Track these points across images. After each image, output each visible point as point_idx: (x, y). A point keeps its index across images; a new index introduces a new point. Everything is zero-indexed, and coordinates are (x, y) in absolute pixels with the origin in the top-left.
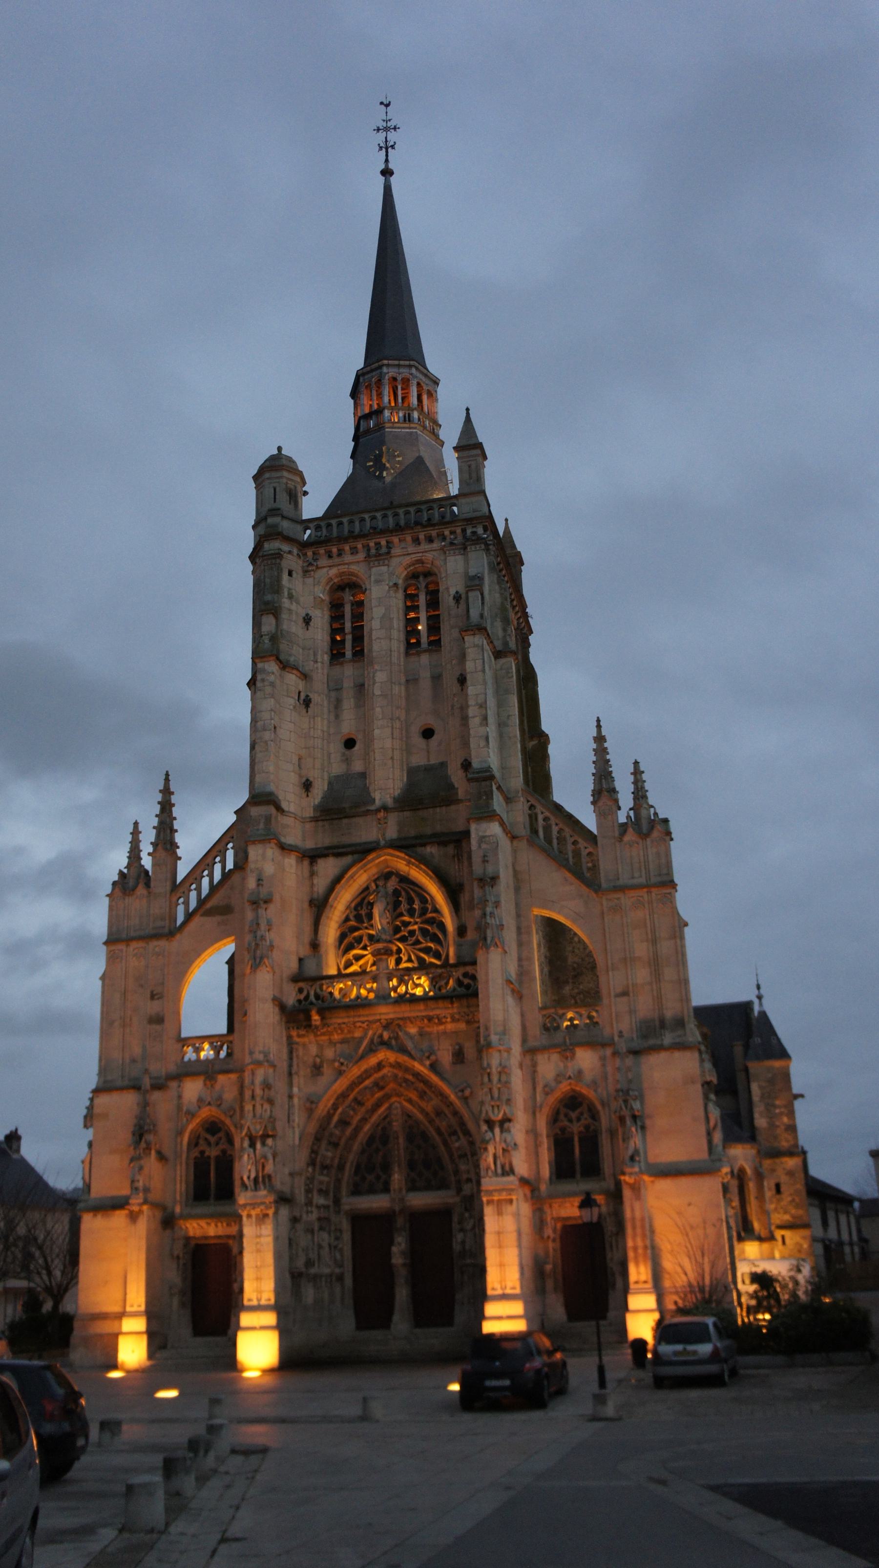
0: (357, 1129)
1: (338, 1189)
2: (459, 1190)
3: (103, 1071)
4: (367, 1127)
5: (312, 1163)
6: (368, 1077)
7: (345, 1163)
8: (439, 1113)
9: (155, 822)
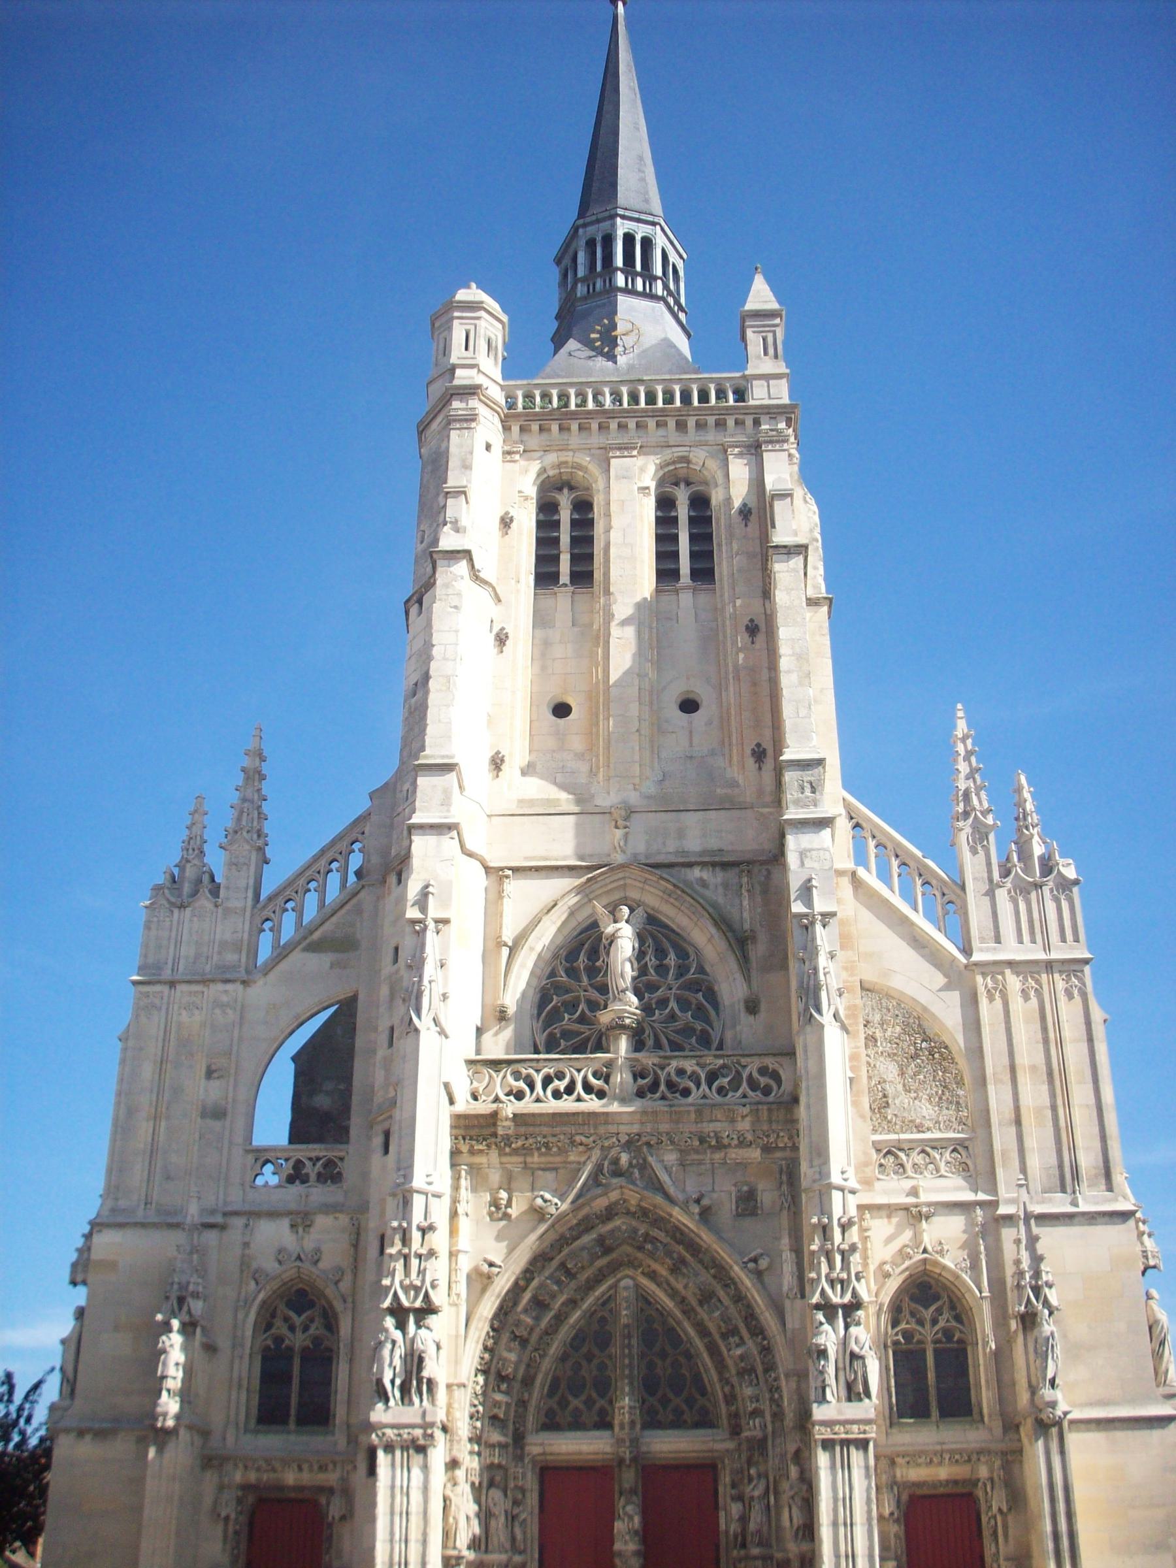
0: (560, 1318)
1: (520, 1418)
2: (735, 1431)
3: (113, 1190)
6: (588, 1230)
7: (536, 1374)
8: (706, 1297)
9: (234, 797)
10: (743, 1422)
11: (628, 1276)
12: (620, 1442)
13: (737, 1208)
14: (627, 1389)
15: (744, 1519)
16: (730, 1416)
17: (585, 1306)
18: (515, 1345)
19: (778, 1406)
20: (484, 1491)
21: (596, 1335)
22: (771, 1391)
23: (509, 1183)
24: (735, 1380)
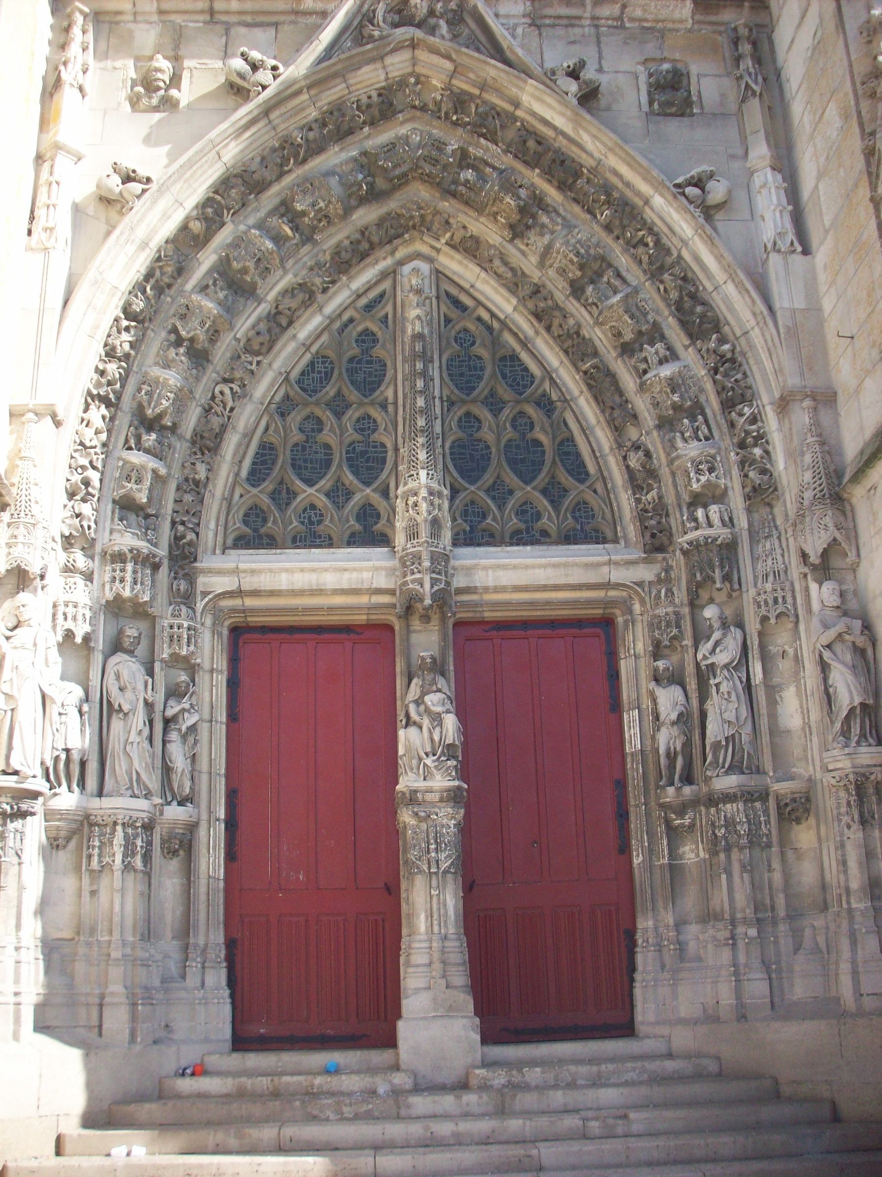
1: (188, 515)
2: (657, 543)
4: (309, 325)
7: (224, 428)
8: (591, 273)
10: (674, 522)
11: (418, 256)
12: (409, 562)
13: (651, 103)
14: (422, 455)
15: (692, 721)
16: (642, 515)
17: (330, 308)
18: (180, 355)
19: (764, 471)
20: (98, 658)
21: (354, 365)
22: (742, 445)
23: (177, 47)
24: (654, 441)
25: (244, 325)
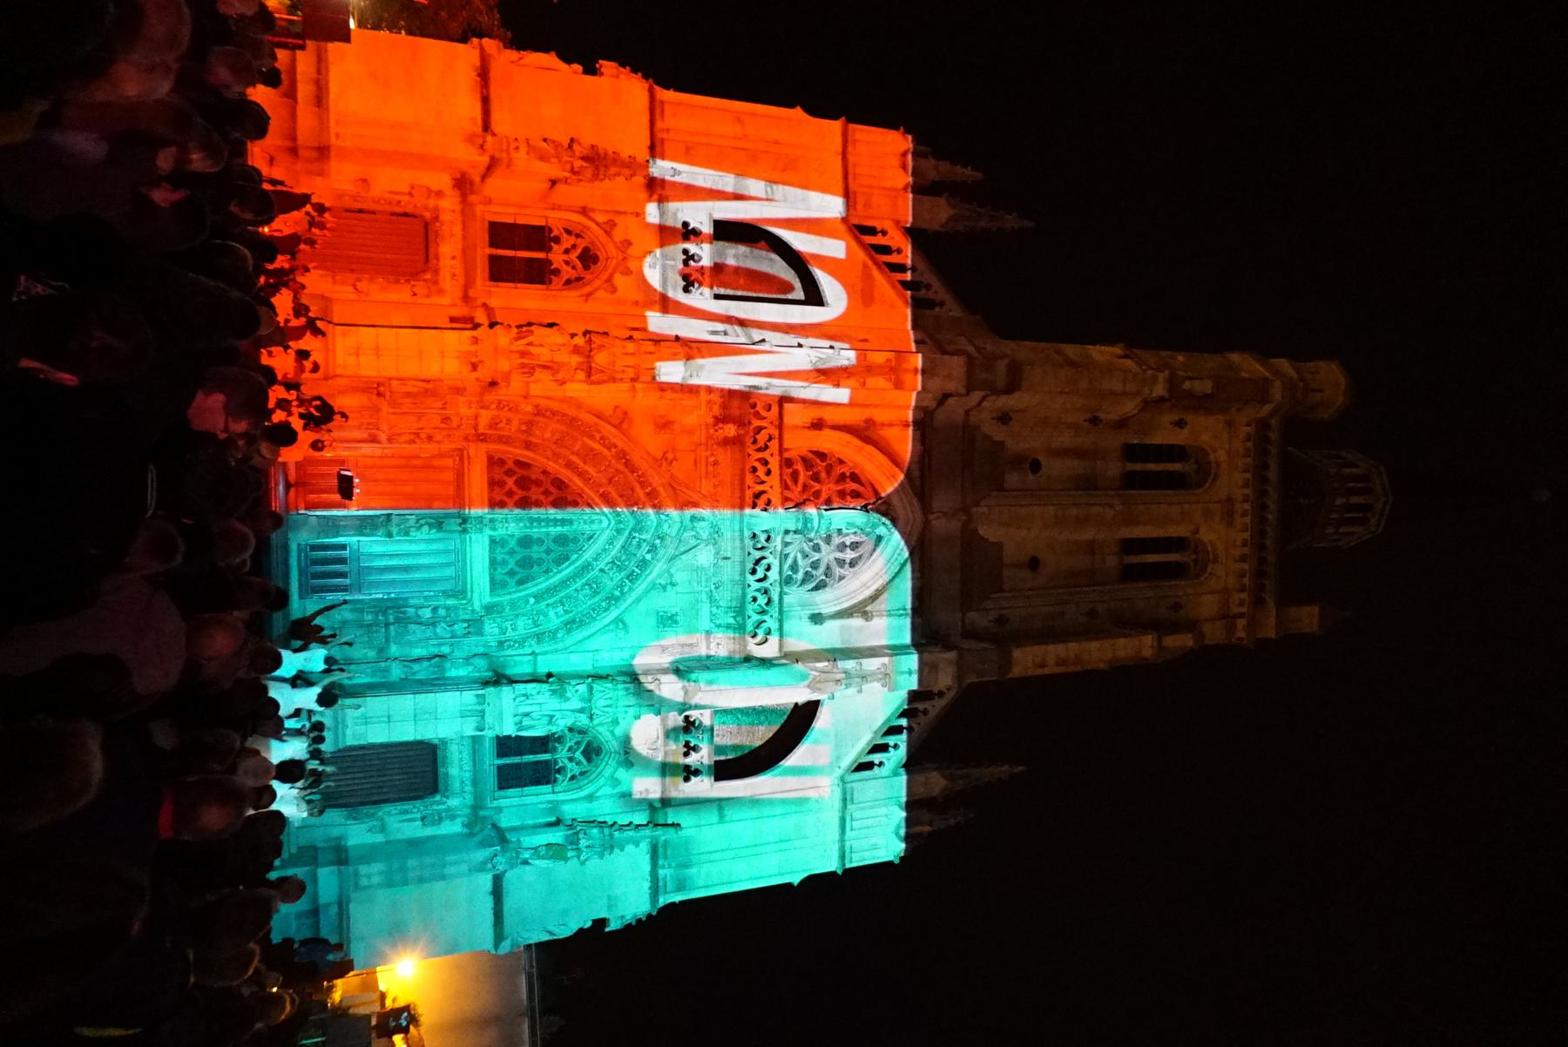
1: (501, 440)
4: (578, 482)
5: (539, 412)
18: (557, 436)
25: (574, 459)
